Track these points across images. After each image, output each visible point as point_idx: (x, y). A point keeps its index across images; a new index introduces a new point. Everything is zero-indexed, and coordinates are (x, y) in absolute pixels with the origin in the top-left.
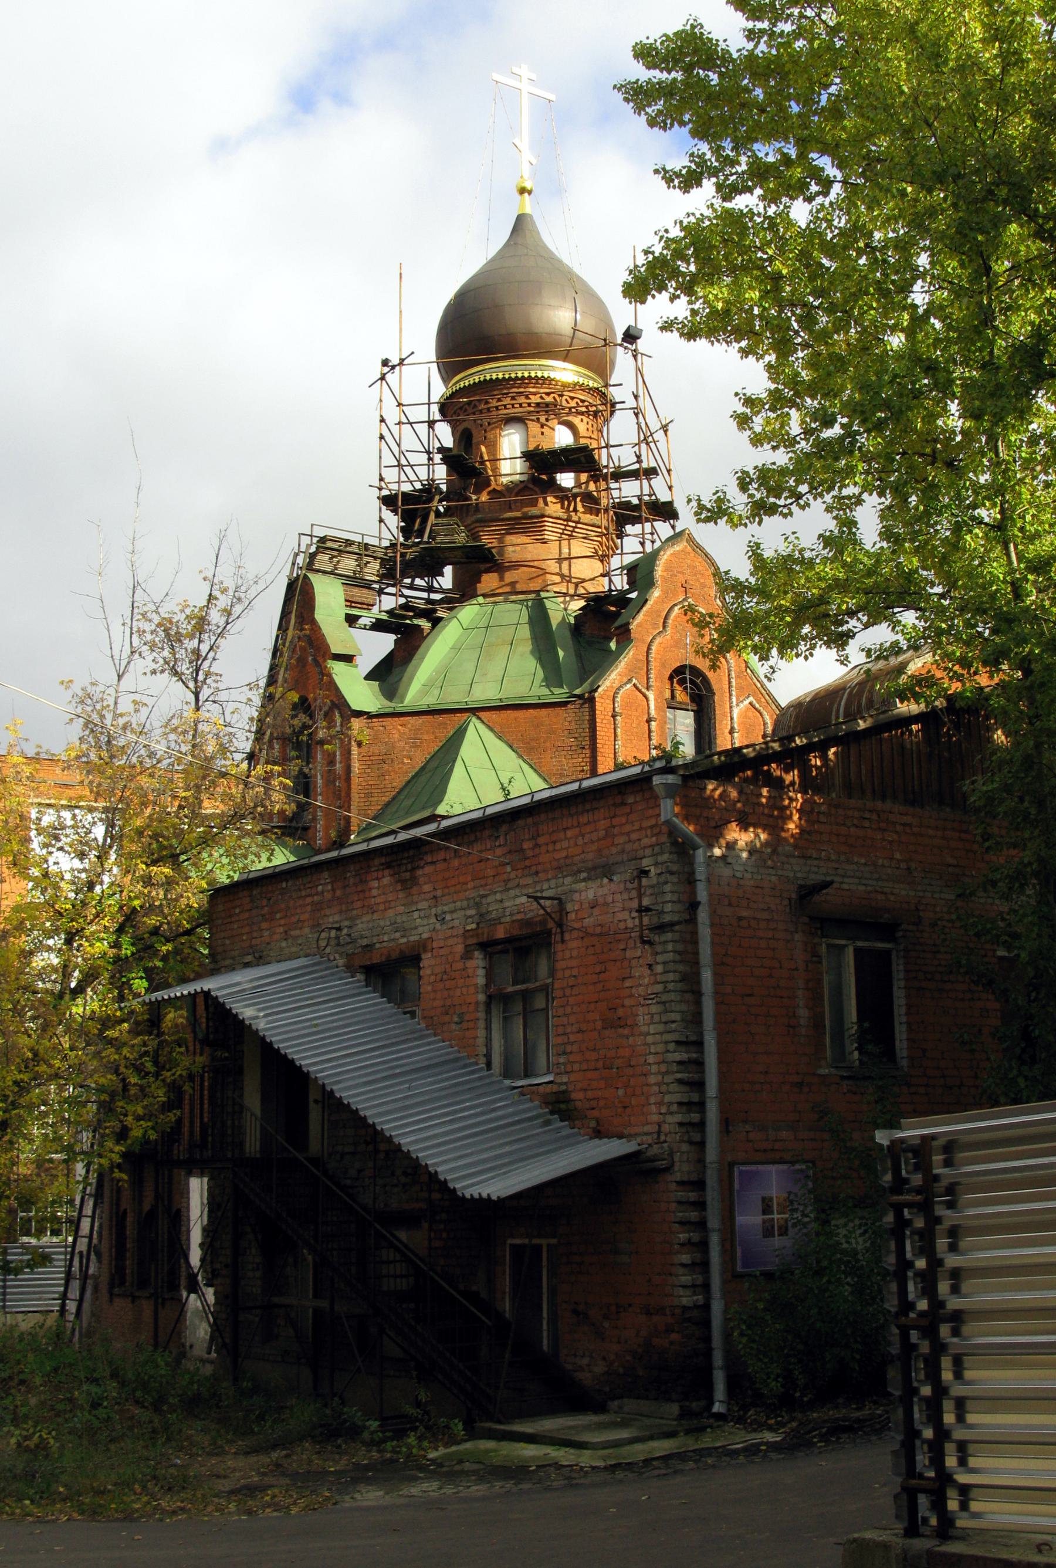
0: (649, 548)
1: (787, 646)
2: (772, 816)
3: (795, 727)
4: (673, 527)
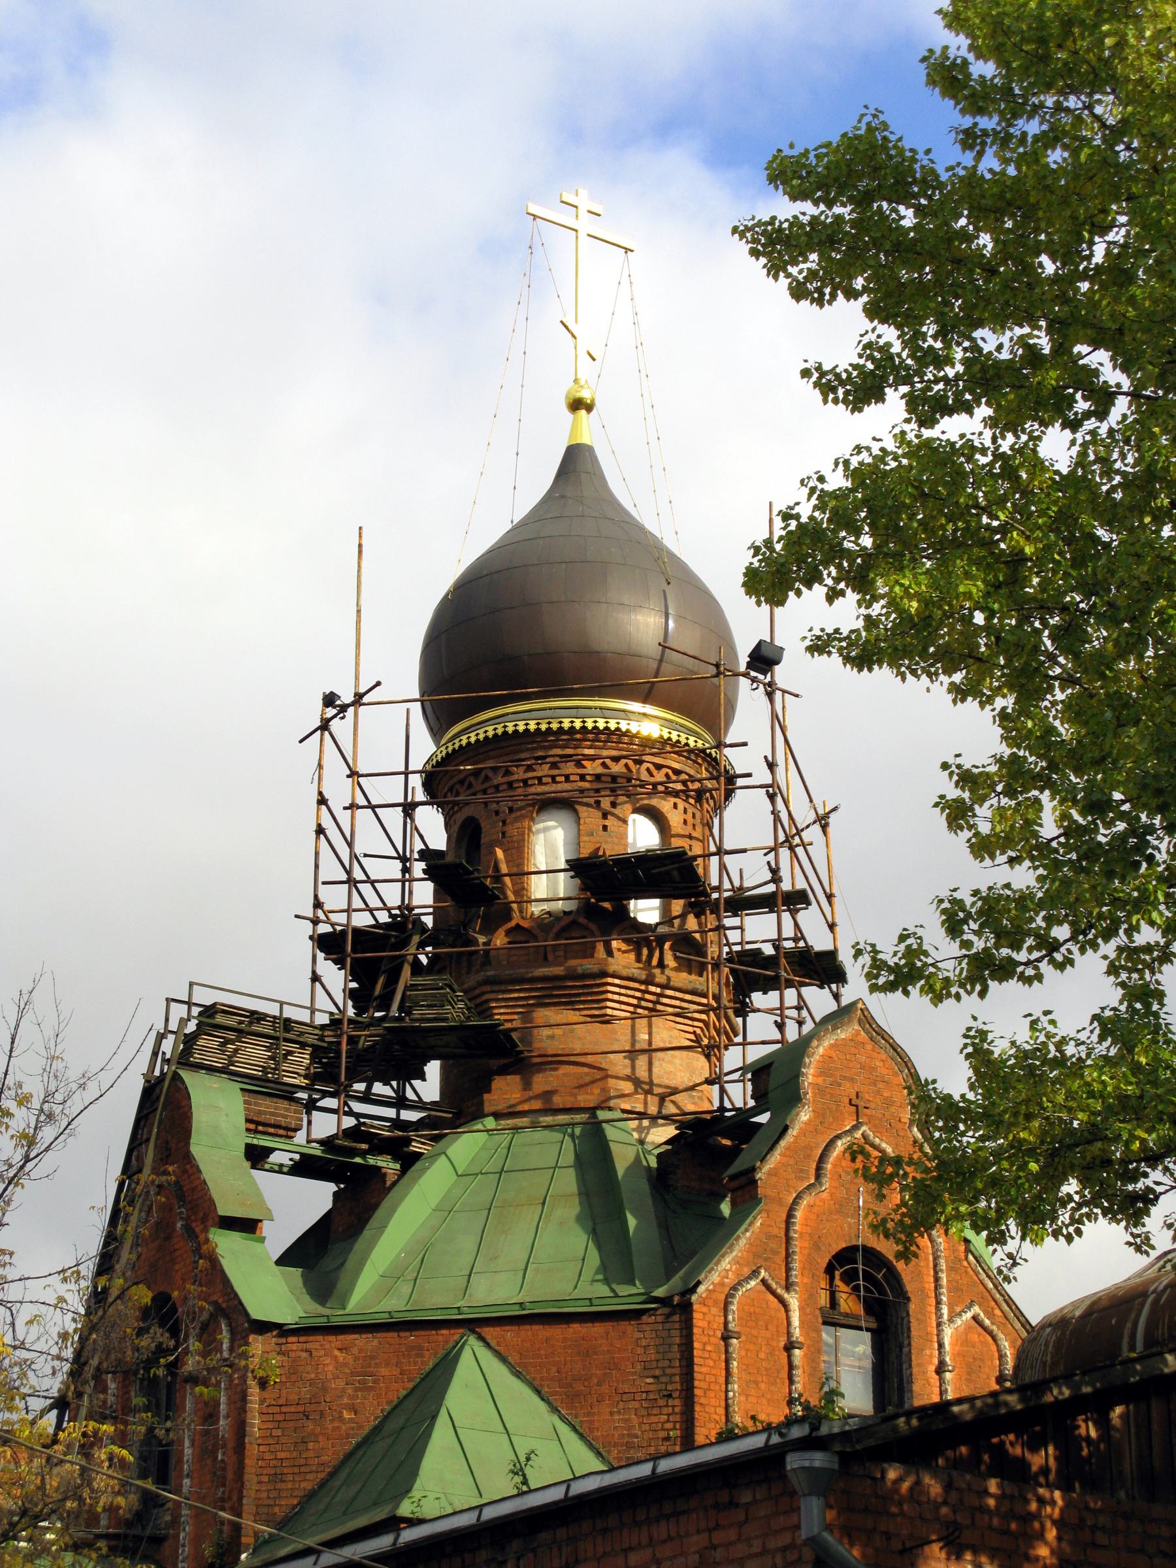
0: (792, 1033)
1: (1036, 1217)
2: (1006, 1532)
3: (1054, 1364)
4: (836, 997)
